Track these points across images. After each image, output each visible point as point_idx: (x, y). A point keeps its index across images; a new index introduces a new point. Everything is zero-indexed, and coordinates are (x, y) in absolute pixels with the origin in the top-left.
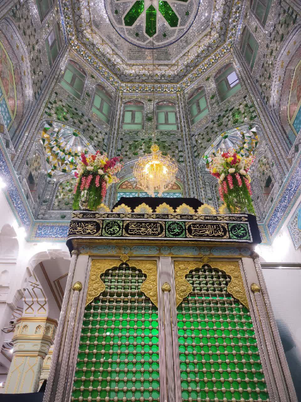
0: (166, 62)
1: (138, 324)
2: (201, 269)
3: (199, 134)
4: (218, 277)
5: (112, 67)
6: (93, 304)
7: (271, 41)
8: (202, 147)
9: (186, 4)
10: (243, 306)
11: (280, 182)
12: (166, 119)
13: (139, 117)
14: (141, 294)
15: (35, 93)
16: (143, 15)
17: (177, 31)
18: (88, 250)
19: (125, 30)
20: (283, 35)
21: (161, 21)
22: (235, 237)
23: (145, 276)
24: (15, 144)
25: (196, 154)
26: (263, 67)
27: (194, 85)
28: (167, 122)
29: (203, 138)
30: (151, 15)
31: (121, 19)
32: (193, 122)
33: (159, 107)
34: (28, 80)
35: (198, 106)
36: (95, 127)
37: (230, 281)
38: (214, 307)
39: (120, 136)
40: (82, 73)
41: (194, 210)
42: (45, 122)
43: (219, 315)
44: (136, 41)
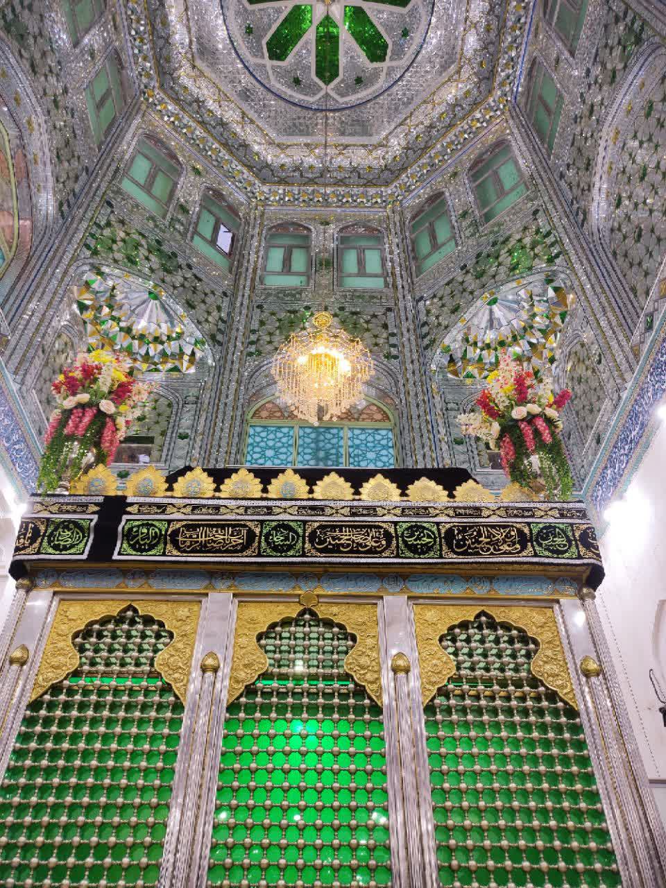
0: (364, 140)
2: (472, 623)
3: (435, 296)
4: (511, 641)
5: (240, 149)
6: (243, 700)
7: (590, 85)
8: (439, 324)
9: (404, 10)
10: (566, 703)
11: (615, 397)
12: (361, 263)
13: (299, 261)
15: (61, 205)
16: (310, 36)
18: (229, 583)
20: (614, 72)
21: (350, 52)
22: (547, 553)
23: (354, 638)
24: (10, 317)
25: (426, 341)
26: (573, 144)
27: (424, 192)
28: (362, 272)
29: (443, 306)
30: (328, 42)
31: (260, 46)
32: (419, 271)
33: (345, 240)
34: (45, 172)
35: (433, 237)
36: (200, 280)
37: (536, 651)
38: (502, 707)
39: (259, 300)
41: (446, 493)
42: (86, 268)
44: (298, 96)
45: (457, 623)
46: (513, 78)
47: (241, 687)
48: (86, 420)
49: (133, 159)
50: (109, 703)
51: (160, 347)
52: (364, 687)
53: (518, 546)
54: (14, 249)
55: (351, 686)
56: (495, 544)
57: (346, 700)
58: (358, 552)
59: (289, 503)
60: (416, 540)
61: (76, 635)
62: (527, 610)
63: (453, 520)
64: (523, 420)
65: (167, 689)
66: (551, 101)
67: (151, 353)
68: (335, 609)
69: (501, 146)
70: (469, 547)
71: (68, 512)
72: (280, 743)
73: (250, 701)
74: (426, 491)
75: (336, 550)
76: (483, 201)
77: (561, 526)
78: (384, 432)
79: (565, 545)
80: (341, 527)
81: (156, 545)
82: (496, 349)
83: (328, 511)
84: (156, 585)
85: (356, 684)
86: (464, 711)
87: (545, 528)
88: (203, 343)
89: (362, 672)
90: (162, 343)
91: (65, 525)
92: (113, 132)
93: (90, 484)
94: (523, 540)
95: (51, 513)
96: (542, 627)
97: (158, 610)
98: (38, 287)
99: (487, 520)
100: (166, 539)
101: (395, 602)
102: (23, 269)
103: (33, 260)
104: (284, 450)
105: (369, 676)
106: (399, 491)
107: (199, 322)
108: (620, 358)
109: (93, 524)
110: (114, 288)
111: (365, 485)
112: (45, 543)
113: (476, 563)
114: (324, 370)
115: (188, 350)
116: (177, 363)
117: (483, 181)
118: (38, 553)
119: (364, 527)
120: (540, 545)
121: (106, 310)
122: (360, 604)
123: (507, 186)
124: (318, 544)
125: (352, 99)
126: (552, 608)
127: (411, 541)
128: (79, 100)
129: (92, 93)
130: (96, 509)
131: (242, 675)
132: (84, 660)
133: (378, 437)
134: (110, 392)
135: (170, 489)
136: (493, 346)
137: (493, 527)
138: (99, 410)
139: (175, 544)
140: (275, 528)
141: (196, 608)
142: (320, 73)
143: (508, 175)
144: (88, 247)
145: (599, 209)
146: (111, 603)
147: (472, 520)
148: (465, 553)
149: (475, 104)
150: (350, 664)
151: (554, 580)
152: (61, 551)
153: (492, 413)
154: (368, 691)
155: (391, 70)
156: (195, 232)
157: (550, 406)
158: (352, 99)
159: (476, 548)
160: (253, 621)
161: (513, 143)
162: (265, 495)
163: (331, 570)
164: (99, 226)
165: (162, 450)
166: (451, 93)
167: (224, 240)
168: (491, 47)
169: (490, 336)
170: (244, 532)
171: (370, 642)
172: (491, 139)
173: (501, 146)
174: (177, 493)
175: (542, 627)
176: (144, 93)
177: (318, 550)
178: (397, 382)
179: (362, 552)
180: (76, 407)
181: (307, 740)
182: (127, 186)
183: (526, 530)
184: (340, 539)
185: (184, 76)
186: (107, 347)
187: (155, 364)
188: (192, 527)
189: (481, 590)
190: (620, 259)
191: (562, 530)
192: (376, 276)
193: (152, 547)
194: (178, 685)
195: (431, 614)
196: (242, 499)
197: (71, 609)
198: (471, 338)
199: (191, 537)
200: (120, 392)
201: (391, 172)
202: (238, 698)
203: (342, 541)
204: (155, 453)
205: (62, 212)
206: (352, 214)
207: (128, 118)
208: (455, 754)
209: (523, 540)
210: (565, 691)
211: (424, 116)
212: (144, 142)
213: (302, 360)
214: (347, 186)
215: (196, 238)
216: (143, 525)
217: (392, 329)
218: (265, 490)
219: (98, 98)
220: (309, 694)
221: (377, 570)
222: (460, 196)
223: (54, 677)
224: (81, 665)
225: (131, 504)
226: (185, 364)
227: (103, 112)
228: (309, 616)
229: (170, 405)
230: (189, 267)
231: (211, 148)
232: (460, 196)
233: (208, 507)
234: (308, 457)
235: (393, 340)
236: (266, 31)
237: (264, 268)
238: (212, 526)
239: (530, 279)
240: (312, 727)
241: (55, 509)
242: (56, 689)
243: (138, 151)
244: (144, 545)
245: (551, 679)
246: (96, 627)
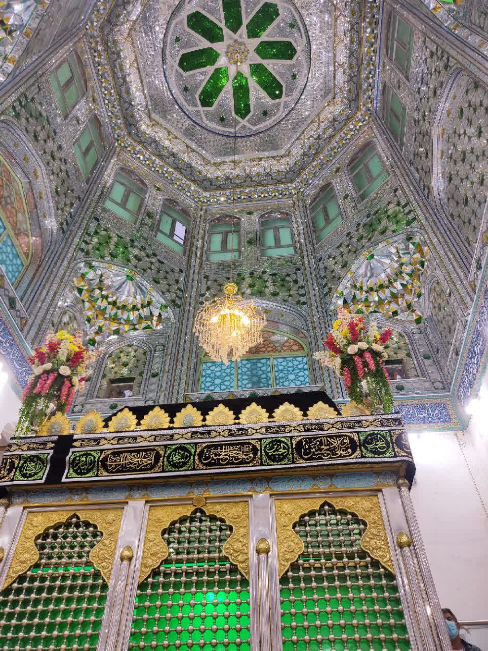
0: (275, 153)
1: (309, 619)
5: (187, 170)
12: (277, 240)
14: (363, 554)
15: (61, 224)
17: (282, 105)
18: (143, 492)
19: (202, 113)
21: (257, 95)
22: (370, 455)
27: (319, 182)
28: (278, 244)
30: (241, 91)
32: (318, 239)
33: (265, 223)
34: (48, 204)
37: (364, 530)
40: (141, 186)
42: (82, 265)
43: (359, 587)
45: (306, 512)
46: (372, 99)
47: (148, 571)
48: (49, 382)
49: (112, 187)
50: (57, 586)
51: (137, 313)
52: (236, 566)
53: (350, 450)
54: (30, 257)
55: (228, 565)
56: (333, 451)
57: (321, 572)
58: (233, 463)
59: (185, 431)
60: (274, 452)
61: (38, 537)
62: (358, 499)
63: (303, 434)
64: (355, 355)
65: (97, 575)
66: (399, 111)
67: (132, 318)
68: (218, 507)
69: (368, 147)
70: (314, 454)
71: (34, 449)
72: (198, 610)
73: (154, 582)
74: (288, 413)
75: (217, 464)
76: (358, 186)
77: (382, 433)
78: (300, 359)
79: (384, 448)
80: (221, 446)
81: (92, 469)
82: (377, 291)
83: (213, 434)
84: (92, 498)
85: (232, 564)
86: (356, 577)
87: (370, 435)
88: (166, 307)
89: (236, 555)
90: (138, 310)
91: (31, 459)
92: (97, 168)
93: (52, 426)
94: (353, 446)
95: (23, 450)
96: (369, 511)
97: (93, 516)
98: (47, 282)
99: (328, 432)
100: (98, 464)
101: (261, 496)
102: (37, 270)
103: (43, 265)
104: (227, 378)
105: (240, 558)
106: (268, 414)
107: (163, 293)
108: (463, 292)
109: (49, 457)
110: (102, 276)
111: (243, 411)
112: (18, 473)
113: (320, 465)
114: (232, 325)
115: (156, 313)
116: (149, 323)
117: (358, 172)
118: (13, 480)
119: (237, 444)
120: (366, 448)
121: (97, 292)
122: (235, 502)
123: (375, 174)
124: (205, 460)
125: (262, 126)
126: (377, 496)
127: (271, 452)
128: (74, 154)
129: (80, 146)
130: (53, 445)
131: (150, 562)
132: (171, 550)
133: (296, 363)
134: (68, 360)
135: (106, 426)
136: (375, 288)
137: (331, 437)
138: (59, 375)
139: (105, 467)
140: (175, 450)
141: (120, 513)
142: (237, 111)
143: (375, 166)
144: (82, 250)
145: (438, 184)
146: (61, 513)
147: (314, 433)
148: (311, 459)
149: (348, 119)
150: (227, 549)
151: (378, 474)
152: (28, 477)
153: (338, 351)
154: (240, 569)
155: (286, 105)
156: (159, 230)
157: (376, 341)
158: (262, 126)
159: (319, 454)
160: (159, 521)
161: (378, 146)
162: (171, 425)
163: (216, 478)
164: (89, 234)
165: (140, 387)
166: (328, 113)
167: (180, 230)
168: (354, 79)
169: (372, 282)
170: (153, 453)
171: (242, 531)
172: (361, 142)
173: (368, 147)
174: (111, 429)
175: (369, 511)
176: (118, 140)
177: (204, 464)
178: (306, 321)
179: (236, 464)
180: (43, 374)
181: (217, 607)
182: (109, 205)
183: (356, 439)
184: (220, 455)
185: (144, 127)
186: (100, 316)
187: (134, 325)
188: (117, 453)
189: (323, 486)
190: (457, 219)
191: (382, 436)
192: (287, 246)
193: (89, 471)
194: (105, 571)
195: (287, 506)
196: (157, 430)
197: (35, 519)
198: (358, 285)
199: (115, 461)
200: (75, 360)
201: (293, 173)
202: (146, 579)
203: (221, 457)
204: (135, 388)
205: (63, 229)
206: (271, 204)
207: (107, 159)
208: (326, 612)
209: (353, 446)
210: (385, 560)
211: (312, 132)
212: (119, 173)
213: (215, 319)
214: (263, 185)
215: (159, 234)
216: (83, 455)
217: (301, 283)
218: (172, 422)
219: (84, 149)
220: (315, 569)
221: (247, 476)
222: (342, 185)
223: (20, 569)
224: (169, 555)
225: (76, 440)
226: (155, 323)
227: (88, 159)
228: (200, 513)
229: (145, 353)
230: (155, 255)
231: (166, 172)
232: (342, 185)
233: (129, 438)
234: (245, 382)
235: (302, 292)
236: (197, 88)
237: (209, 249)
238: (131, 452)
239: (396, 239)
240: (222, 597)
241: (25, 448)
242: (21, 579)
243: (115, 181)
244: (84, 469)
245: (375, 551)
246: (52, 531)
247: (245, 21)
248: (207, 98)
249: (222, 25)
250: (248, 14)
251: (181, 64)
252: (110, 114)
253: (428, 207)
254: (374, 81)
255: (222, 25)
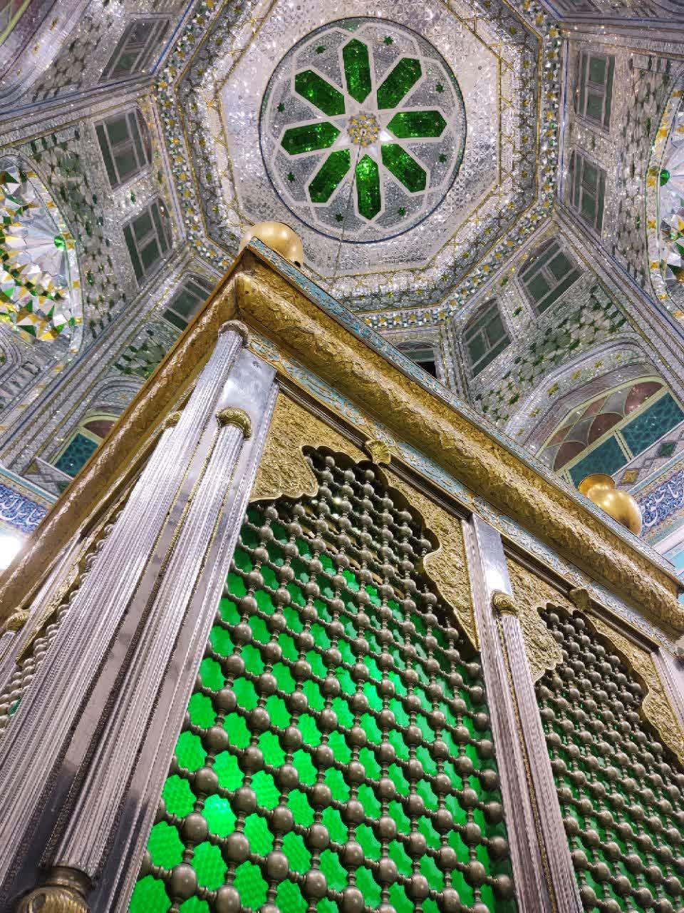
247: (376, 84)
248: (321, 188)
249: (344, 91)
250: (372, 99)
251: (285, 144)
252: (187, 222)
253: (645, 299)
254: (557, 156)
255: (344, 91)
